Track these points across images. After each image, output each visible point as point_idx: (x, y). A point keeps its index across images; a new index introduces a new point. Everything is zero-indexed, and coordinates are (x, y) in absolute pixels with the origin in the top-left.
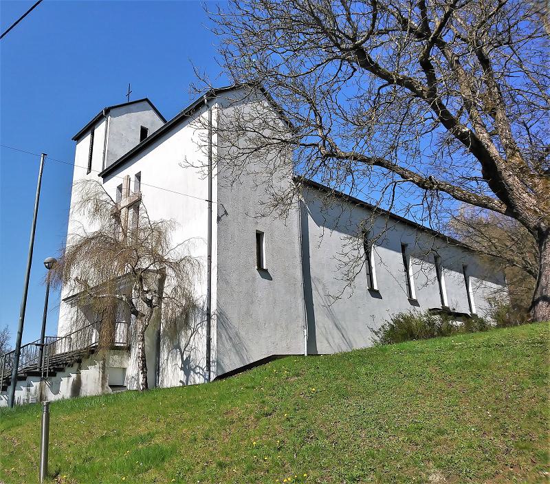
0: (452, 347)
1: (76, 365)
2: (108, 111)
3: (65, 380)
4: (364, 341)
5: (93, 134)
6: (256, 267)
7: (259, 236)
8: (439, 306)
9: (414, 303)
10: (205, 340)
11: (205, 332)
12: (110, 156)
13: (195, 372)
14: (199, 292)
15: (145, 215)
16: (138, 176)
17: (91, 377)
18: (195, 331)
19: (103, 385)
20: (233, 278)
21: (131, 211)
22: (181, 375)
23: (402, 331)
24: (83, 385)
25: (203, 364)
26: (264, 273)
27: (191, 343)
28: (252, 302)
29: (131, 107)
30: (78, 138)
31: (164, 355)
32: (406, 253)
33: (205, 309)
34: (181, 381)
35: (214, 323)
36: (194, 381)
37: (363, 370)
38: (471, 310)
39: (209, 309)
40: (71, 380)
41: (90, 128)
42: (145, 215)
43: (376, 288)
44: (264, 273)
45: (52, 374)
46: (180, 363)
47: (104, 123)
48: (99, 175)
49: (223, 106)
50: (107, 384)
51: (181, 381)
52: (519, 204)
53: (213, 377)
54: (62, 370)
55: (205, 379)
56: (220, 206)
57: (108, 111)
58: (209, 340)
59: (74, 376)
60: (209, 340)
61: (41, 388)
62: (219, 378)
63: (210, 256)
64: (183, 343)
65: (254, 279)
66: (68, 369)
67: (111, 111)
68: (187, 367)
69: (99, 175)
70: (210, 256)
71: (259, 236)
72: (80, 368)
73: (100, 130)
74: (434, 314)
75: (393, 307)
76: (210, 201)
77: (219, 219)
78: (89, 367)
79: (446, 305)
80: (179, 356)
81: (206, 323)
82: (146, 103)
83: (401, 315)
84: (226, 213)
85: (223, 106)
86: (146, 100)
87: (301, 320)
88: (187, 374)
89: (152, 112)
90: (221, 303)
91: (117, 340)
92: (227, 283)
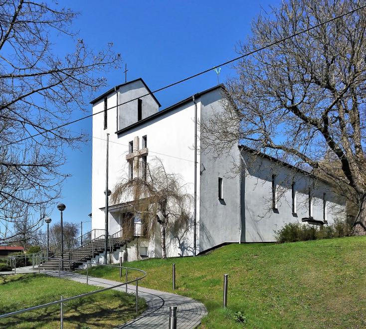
0: (318, 246)
1: (125, 246)
2: (118, 88)
3: (120, 253)
4: (271, 237)
5: (106, 102)
6: (218, 198)
7: (220, 180)
8: (308, 217)
9: (295, 215)
10: (193, 235)
11: (193, 231)
12: (121, 119)
13: (187, 249)
14: (190, 209)
15: (163, 170)
16: (145, 138)
17: (132, 252)
18: (187, 230)
19: (137, 256)
20: (207, 205)
21: (141, 160)
22: (179, 251)
23: (290, 235)
24: (129, 255)
25: (193, 246)
26: (222, 201)
27: (184, 236)
28: (216, 217)
29: (132, 85)
30: (95, 102)
31: (168, 240)
32: (294, 189)
33: (193, 219)
34: (179, 254)
35: (198, 227)
36: (187, 254)
37: (284, 255)
38: (324, 218)
39: (195, 220)
40: (123, 253)
41: (104, 98)
42: (163, 170)
43: (276, 207)
44: (222, 201)
45: (115, 250)
46: (178, 245)
47: (115, 96)
48: (115, 133)
49: (205, 104)
50: (139, 255)
51: (179, 254)
52: (356, 181)
53: (198, 252)
54: (119, 248)
55: (193, 253)
56: (202, 165)
57: (118, 88)
58: (195, 235)
59: (124, 251)
60: (195, 235)
61: (110, 257)
62: (202, 253)
63: (195, 192)
64: (180, 235)
65: (217, 204)
66: (121, 248)
67: (120, 88)
68: (182, 247)
69: (115, 133)
70: (195, 192)
71: (220, 180)
72: (126, 247)
73: (112, 100)
74: (305, 221)
75: (284, 220)
76: (196, 163)
77: (201, 173)
78: (131, 247)
79: (312, 216)
80: (177, 242)
81: (193, 227)
82: (140, 81)
83: (290, 224)
84: (205, 169)
85: (205, 104)
86: (141, 79)
87: (239, 225)
88: (183, 250)
89: (144, 89)
90: (201, 218)
91: (136, 232)
92: (204, 207)
